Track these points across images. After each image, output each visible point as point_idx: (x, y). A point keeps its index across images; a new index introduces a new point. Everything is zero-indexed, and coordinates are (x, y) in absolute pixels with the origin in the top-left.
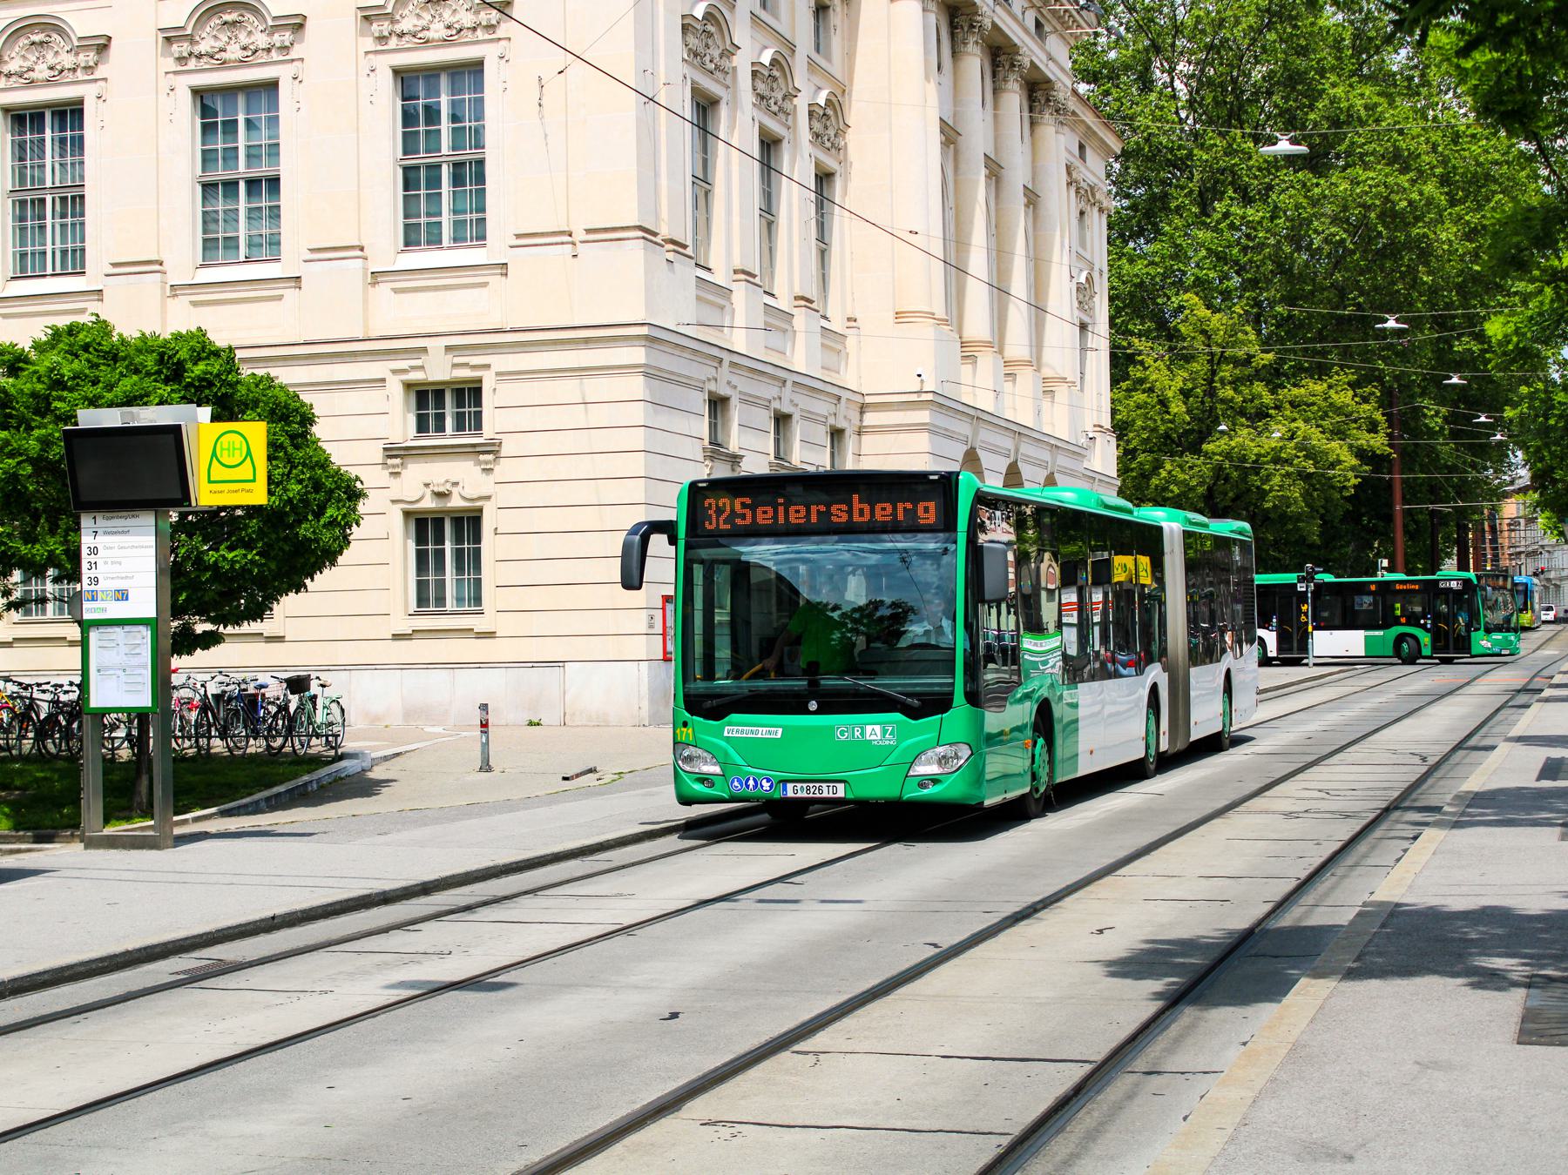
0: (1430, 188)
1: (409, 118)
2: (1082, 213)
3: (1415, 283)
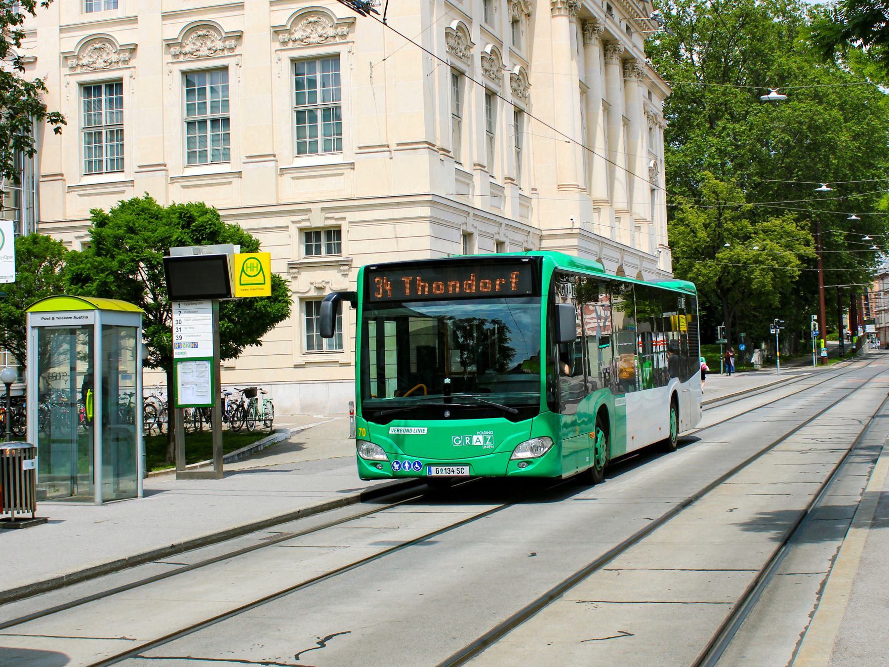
0: (835, 112)
1: (299, 85)
2: (650, 129)
3: (828, 165)
